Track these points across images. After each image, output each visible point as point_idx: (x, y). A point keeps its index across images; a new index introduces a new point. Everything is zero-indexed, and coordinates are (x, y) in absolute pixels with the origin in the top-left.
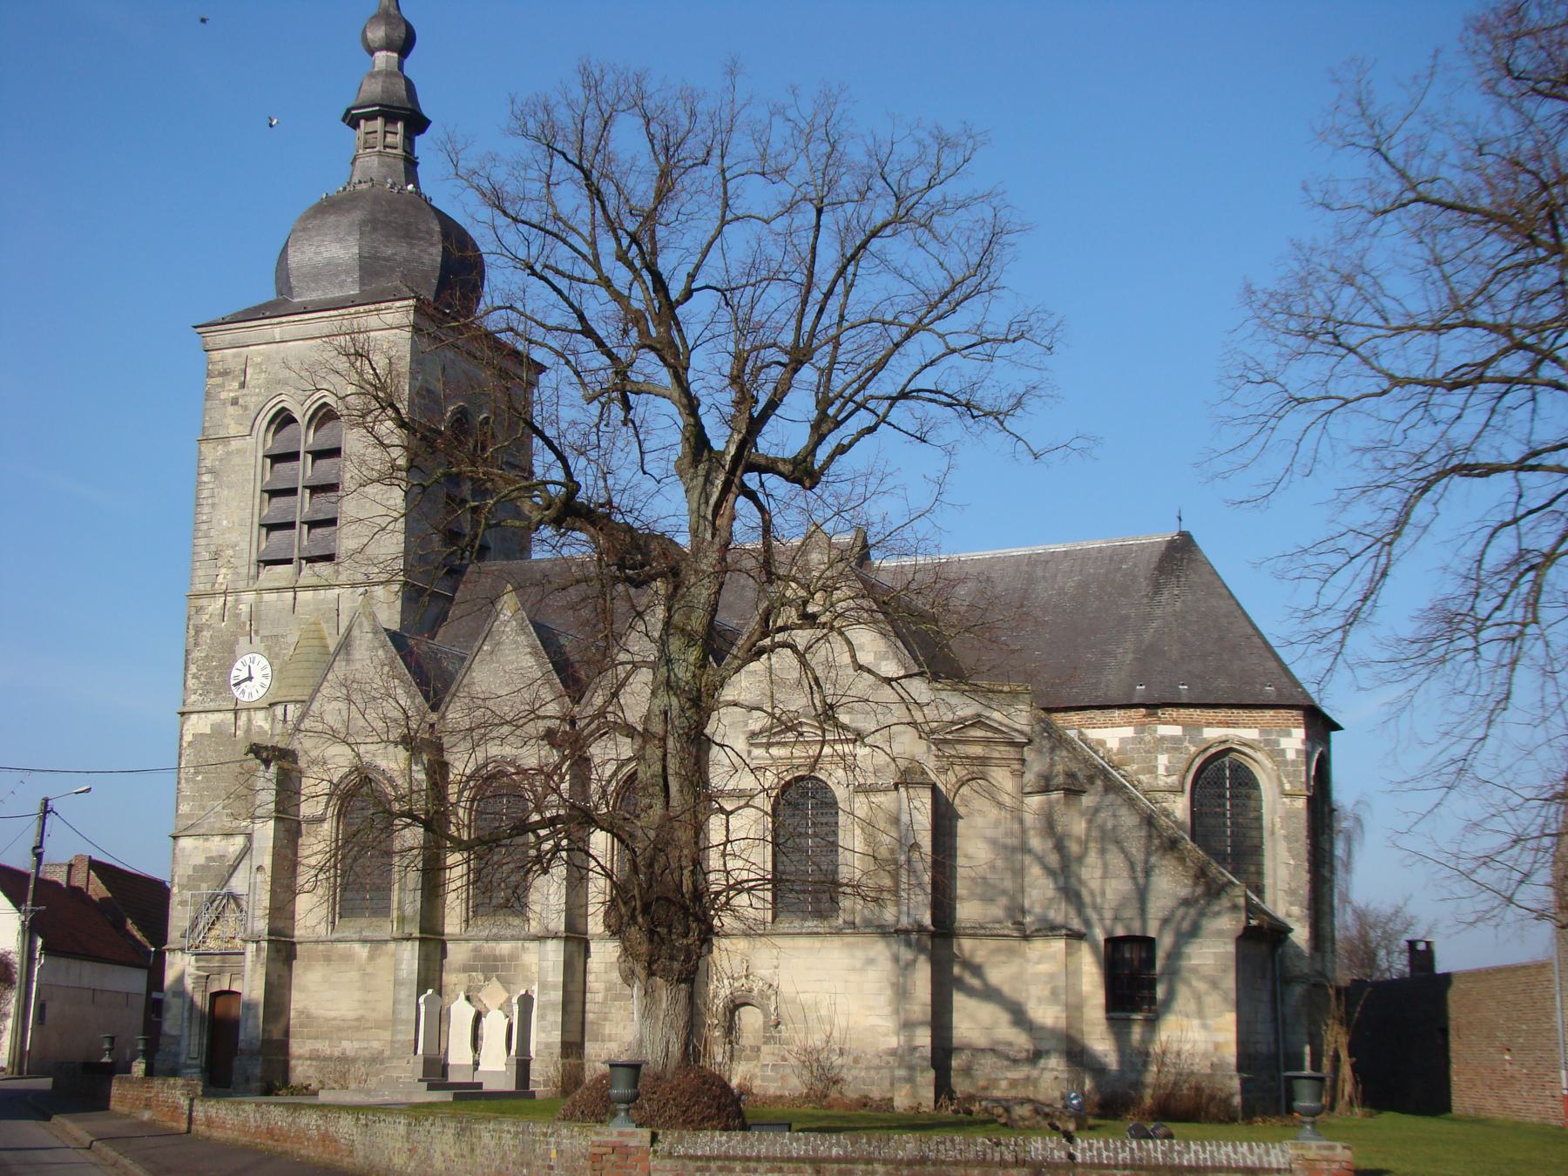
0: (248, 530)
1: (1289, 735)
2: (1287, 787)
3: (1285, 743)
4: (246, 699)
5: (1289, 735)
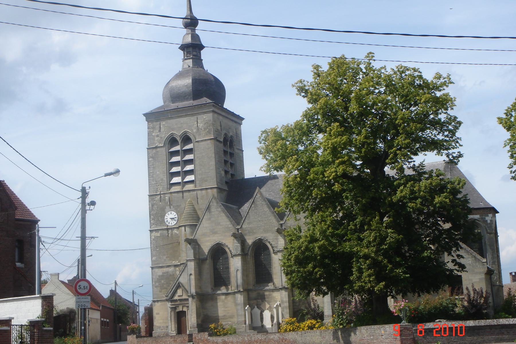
0: (166, 174)
1: (488, 216)
2: (489, 231)
3: (487, 218)
4: (170, 225)
5: (488, 216)
